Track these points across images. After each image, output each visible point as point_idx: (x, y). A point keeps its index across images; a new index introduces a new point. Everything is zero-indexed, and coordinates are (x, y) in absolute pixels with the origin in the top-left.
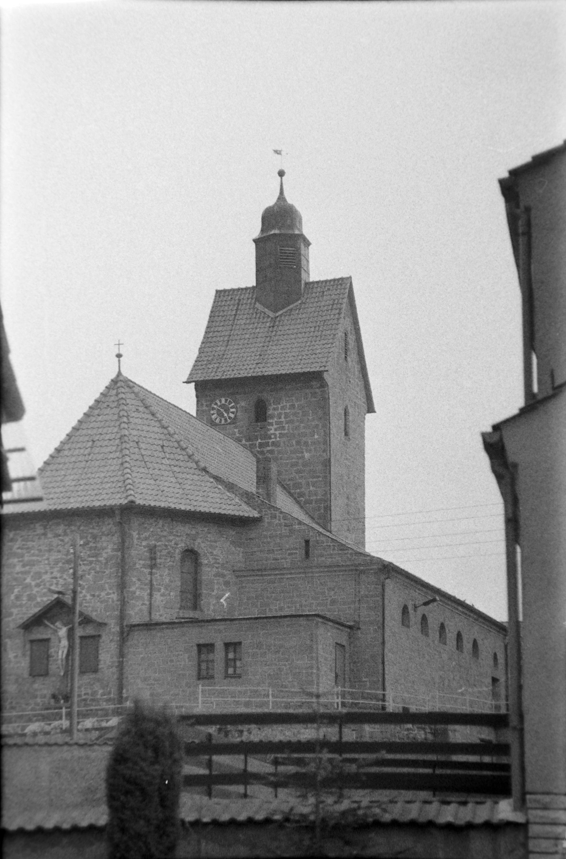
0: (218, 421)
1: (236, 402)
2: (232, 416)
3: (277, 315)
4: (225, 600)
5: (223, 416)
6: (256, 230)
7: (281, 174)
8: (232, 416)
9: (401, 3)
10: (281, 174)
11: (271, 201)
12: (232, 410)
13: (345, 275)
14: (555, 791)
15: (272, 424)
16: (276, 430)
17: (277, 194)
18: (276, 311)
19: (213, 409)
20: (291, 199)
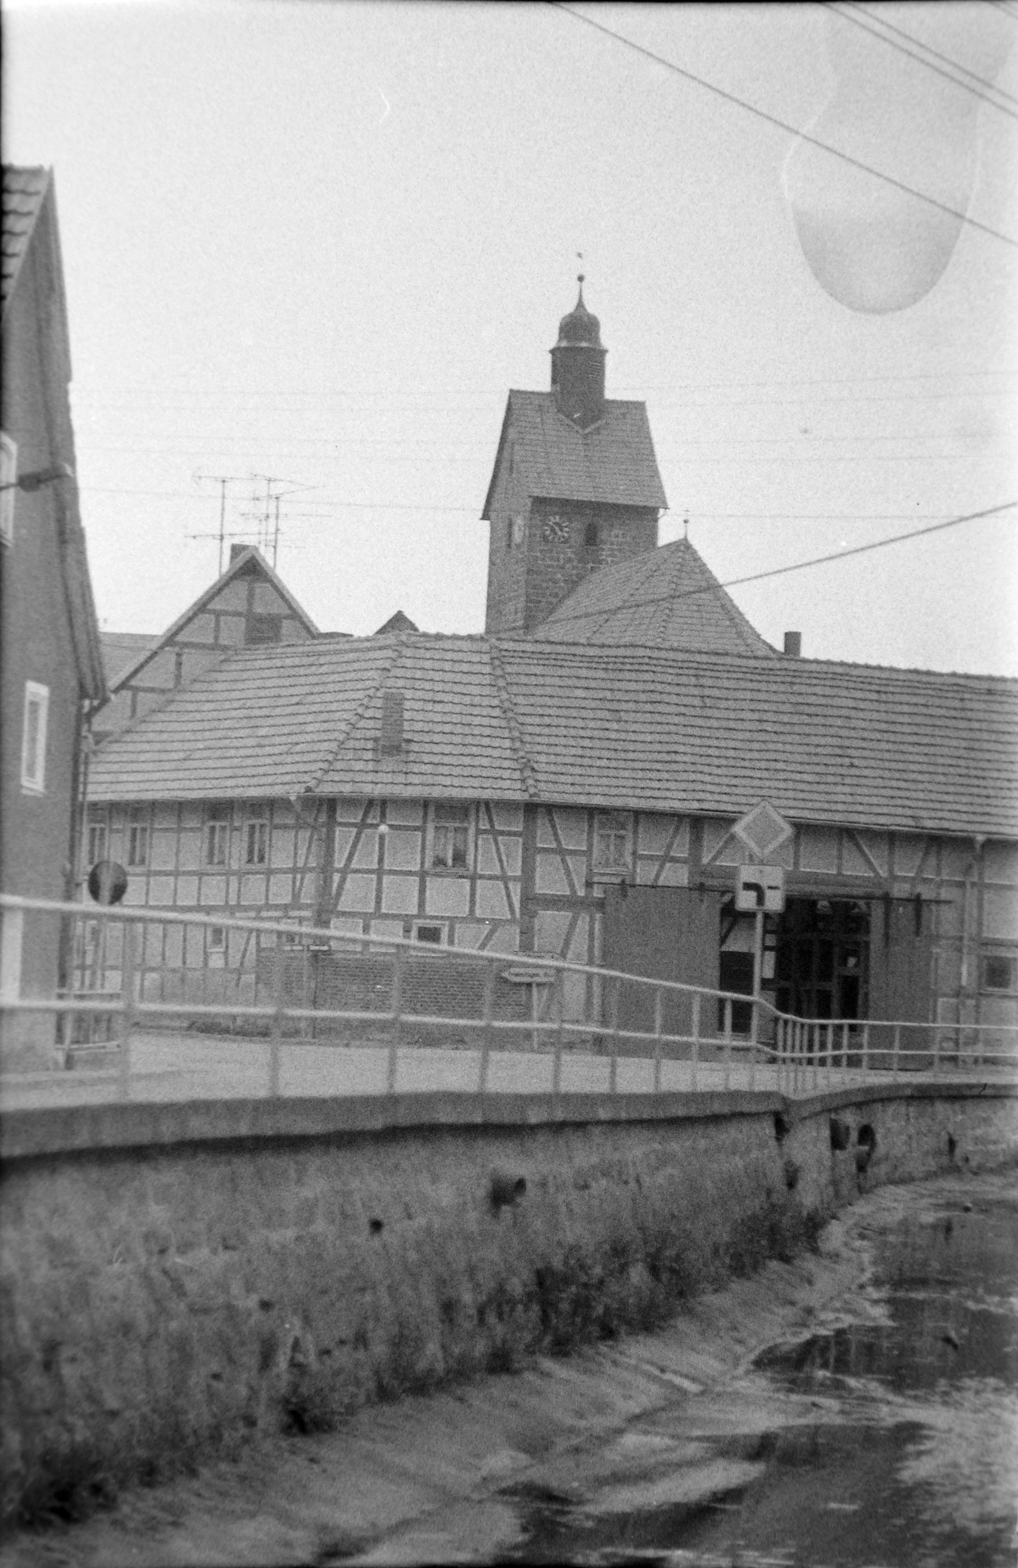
0: (550, 538)
1: (570, 521)
2: (566, 535)
3: (587, 431)
4: (745, 829)
5: (556, 534)
6: (552, 339)
7: (581, 279)
8: (566, 535)
9: (967, 4)
10: (581, 279)
11: (570, 308)
12: (566, 529)
13: (508, 393)
14: (379, 672)
15: (603, 550)
16: (607, 556)
17: (575, 302)
18: (584, 427)
19: (547, 525)
20: (591, 309)
